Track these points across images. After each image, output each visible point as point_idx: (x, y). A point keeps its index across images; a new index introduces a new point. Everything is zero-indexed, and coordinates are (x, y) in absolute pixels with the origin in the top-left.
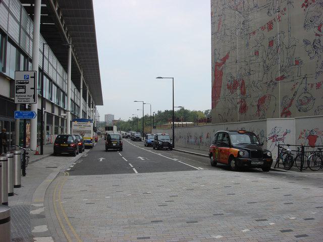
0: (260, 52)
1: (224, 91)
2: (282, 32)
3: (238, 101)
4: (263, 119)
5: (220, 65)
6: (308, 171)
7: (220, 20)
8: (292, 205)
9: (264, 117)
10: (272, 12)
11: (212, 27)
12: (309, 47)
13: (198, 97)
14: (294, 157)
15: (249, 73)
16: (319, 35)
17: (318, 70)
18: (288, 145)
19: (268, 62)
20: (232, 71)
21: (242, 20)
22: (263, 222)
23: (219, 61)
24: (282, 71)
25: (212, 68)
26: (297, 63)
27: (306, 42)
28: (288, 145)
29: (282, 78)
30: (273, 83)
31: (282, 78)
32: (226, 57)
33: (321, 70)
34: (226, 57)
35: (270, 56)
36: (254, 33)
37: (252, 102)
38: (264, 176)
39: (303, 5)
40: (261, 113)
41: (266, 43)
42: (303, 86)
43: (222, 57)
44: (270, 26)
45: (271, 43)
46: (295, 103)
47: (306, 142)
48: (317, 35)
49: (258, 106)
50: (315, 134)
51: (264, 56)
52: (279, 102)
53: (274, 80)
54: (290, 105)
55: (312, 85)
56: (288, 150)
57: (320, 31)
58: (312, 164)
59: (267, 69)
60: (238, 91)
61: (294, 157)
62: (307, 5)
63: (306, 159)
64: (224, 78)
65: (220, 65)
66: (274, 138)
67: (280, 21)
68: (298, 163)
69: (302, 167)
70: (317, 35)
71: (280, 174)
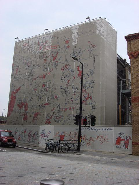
0: (37, 89)
1: (16, 108)
2: (50, 81)
3: (23, 113)
4: (37, 125)
5: (14, 93)
6: (61, 153)
7: (17, 69)
8: (61, 168)
9: (36, 123)
10: (45, 70)
11: (13, 72)
12: (63, 90)
13: (5, 114)
14: (55, 146)
15: (31, 99)
16: (68, 85)
17: (66, 102)
18: (52, 140)
19: (41, 94)
20: (20, 96)
21: (29, 71)
22: (53, 175)
23: (14, 91)
24: (48, 100)
25: (10, 94)
26: (56, 97)
27: (61, 88)
28: (52, 140)
29: (48, 104)
30: (43, 106)
31: (48, 104)
32: (19, 89)
33: (68, 102)
34: (19, 89)
35: (43, 92)
36: (35, 79)
37: (31, 115)
38: (11, 151)
39: (62, 69)
40: (35, 121)
41: (41, 85)
42: (58, 109)
43: (16, 89)
44: (44, 77)
45: (44, 85)
46: (53, 117)
47: (59, 138)
48: (67, 85)
49: (34, 118)
50: (64, 134)
51: (39, 91)
52: (45, 116)
53: (43, 105)
54: (51, 118)
55: (63, 109)
56: (52, 142)
57: (69, 83)
58: (63, 150)
59: (40, 98)
60: (23, 109)
61: (55, 146)
62: (64, 70)
63: (61, 147)
64: (16, 100)
65: (14, 93)
66: (43, 135)
67: (49, 75)
68: (57, 149)
69: (59, 151)
70: (67, 85)
71: (49, 154)
